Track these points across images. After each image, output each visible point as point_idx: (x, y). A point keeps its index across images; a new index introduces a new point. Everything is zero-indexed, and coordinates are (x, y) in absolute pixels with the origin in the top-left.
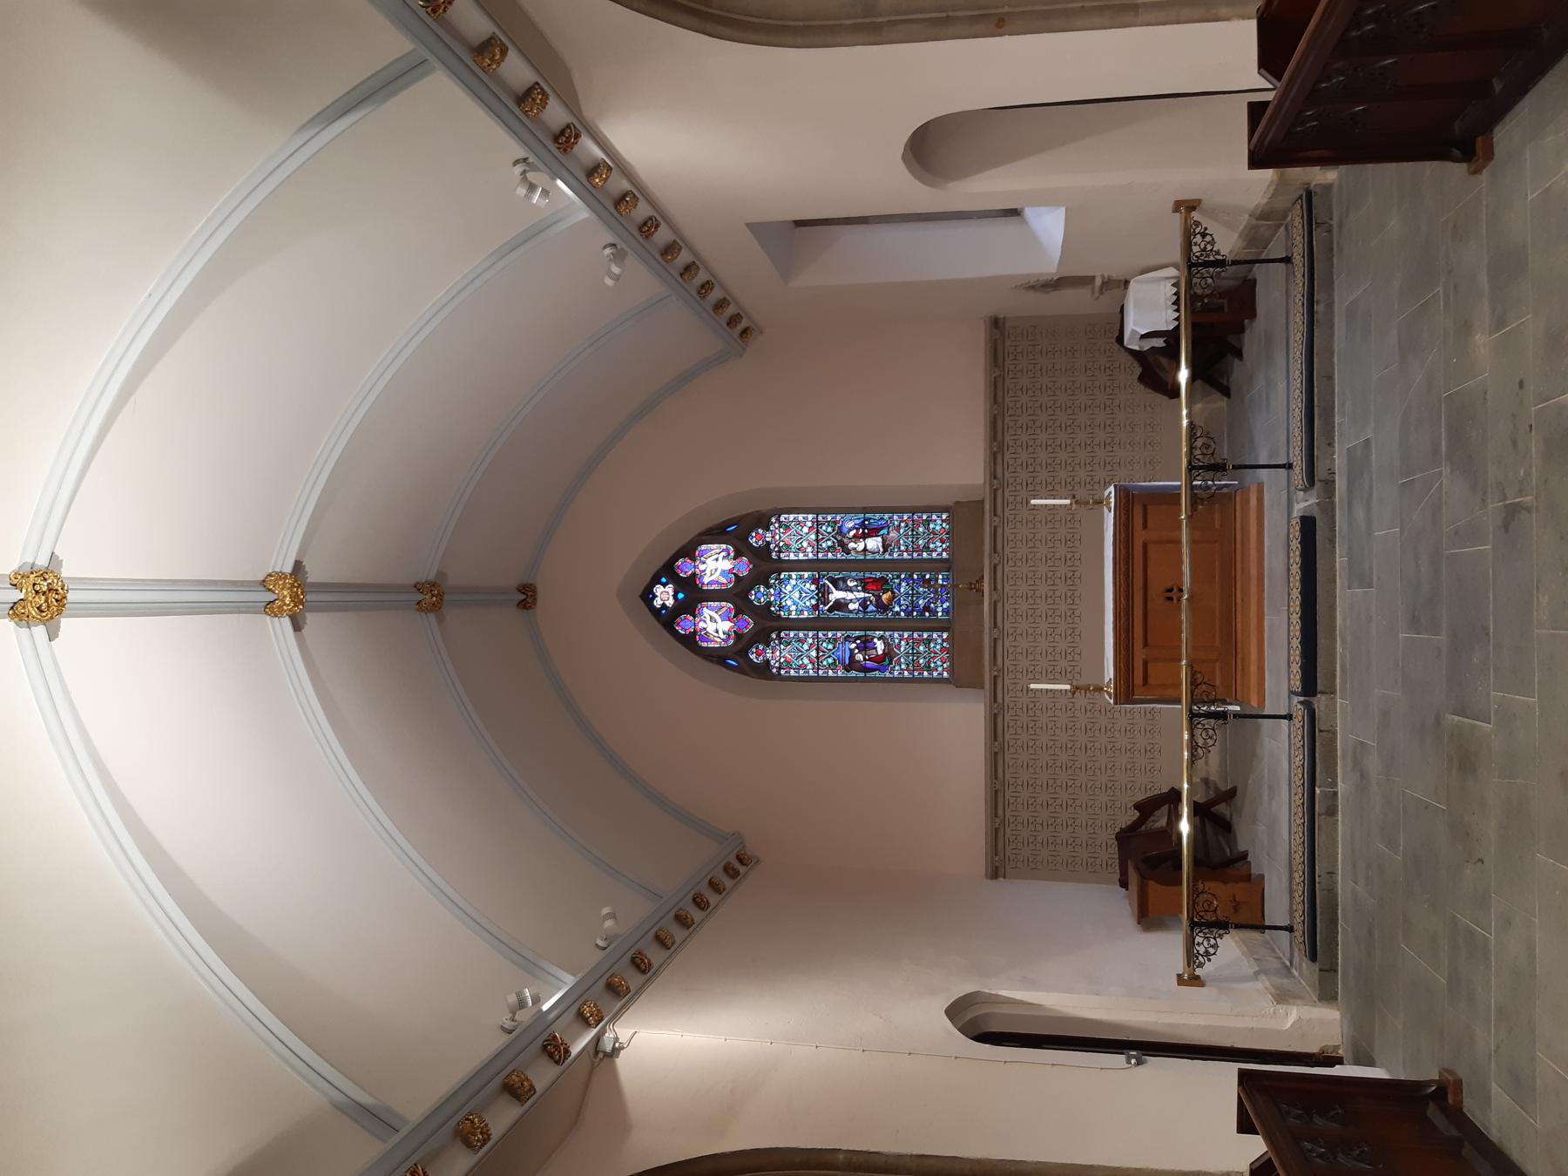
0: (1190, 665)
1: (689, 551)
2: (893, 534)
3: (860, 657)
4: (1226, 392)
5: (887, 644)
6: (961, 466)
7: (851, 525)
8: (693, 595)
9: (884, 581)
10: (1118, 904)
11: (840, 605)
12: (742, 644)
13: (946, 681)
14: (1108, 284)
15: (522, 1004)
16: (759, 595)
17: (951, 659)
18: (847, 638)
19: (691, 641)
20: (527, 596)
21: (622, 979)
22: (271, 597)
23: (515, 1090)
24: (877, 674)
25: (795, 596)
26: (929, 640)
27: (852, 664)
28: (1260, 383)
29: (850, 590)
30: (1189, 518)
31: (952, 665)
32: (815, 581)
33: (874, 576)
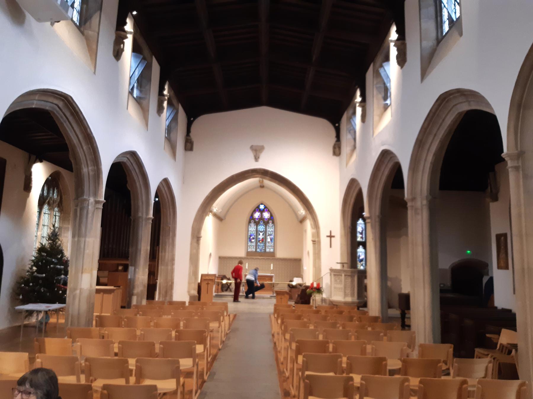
6: (280, 254)
8: (262, 211)
11: (259, 235)
12: (254, 219)
16: (262, 223)
21: (215, 215)
27: (251, 236)
33: (264, 240)
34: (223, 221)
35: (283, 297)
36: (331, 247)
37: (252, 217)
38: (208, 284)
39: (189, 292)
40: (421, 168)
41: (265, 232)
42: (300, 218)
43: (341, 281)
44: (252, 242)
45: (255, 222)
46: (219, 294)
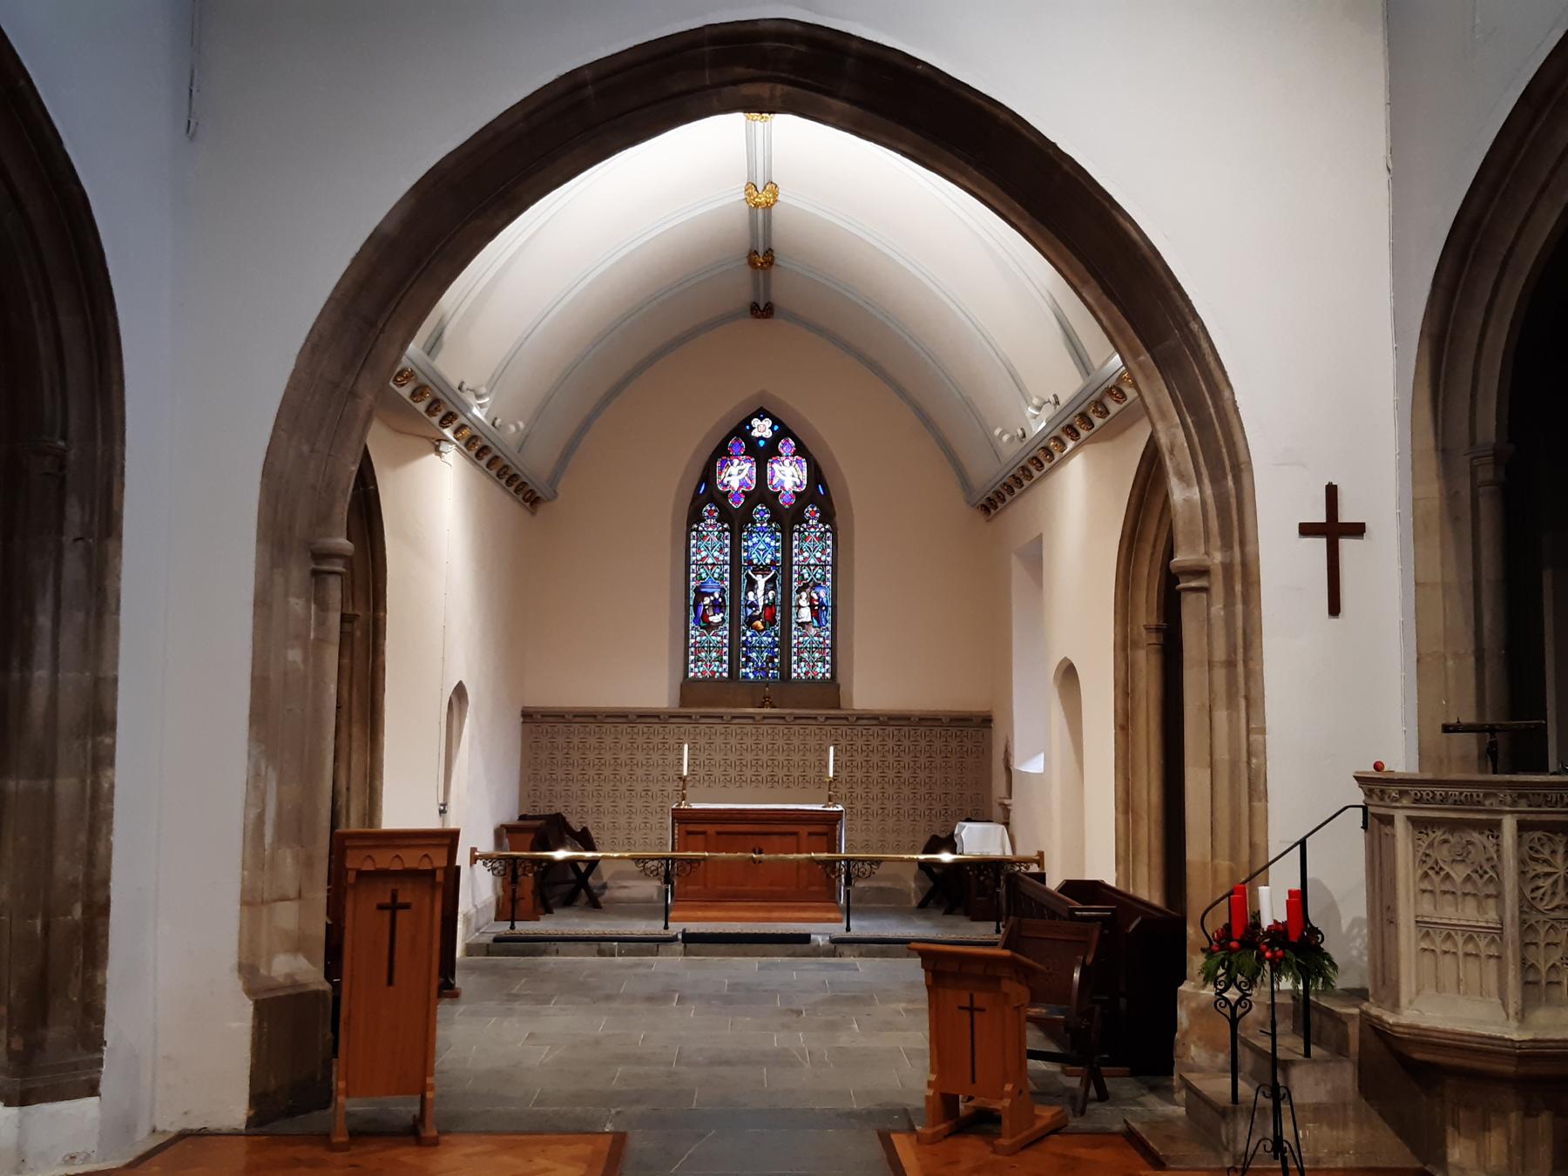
0: (704, 858)
1: (801, 450)
2: (813, 631)
3: (707, 601)
4: (922, 905)
5: (718, 624)
6: (868, 691)
7: (822, 594)
8: (763, 455)
9: (773, 622)
10: (510, 815)
11: (752, 585)
12: (720, 498)
13: (686, 675)
14: (1006, 810)
15: (479, 397)
16: (761, 513)
17: (704, 680)
18: (723, 590)
19: (721, 453)
20: (762, 310)
21: (479, 449)
22: (760, 188)
23: (418, 393)
24: (692, 616)
25: (761, 546)
26: (721, 662)
27: (700, 594)
28: (928, 923)
29: (765, 593)
30: (812, 859)
31: (700, 680)
32: (773, 562)
33: (778, 614)
34: (542, 509)
35: (981, 999)
36: (1334, 608)
37: (705, 495)
38: (394, 907)
39: (248, 970)
40: (1484, 291)
41: (782, 572)
42: (986, 474)
43: (1488, 872)
44: (709, 627)
45: (725, 515)
46: (523, 927)
